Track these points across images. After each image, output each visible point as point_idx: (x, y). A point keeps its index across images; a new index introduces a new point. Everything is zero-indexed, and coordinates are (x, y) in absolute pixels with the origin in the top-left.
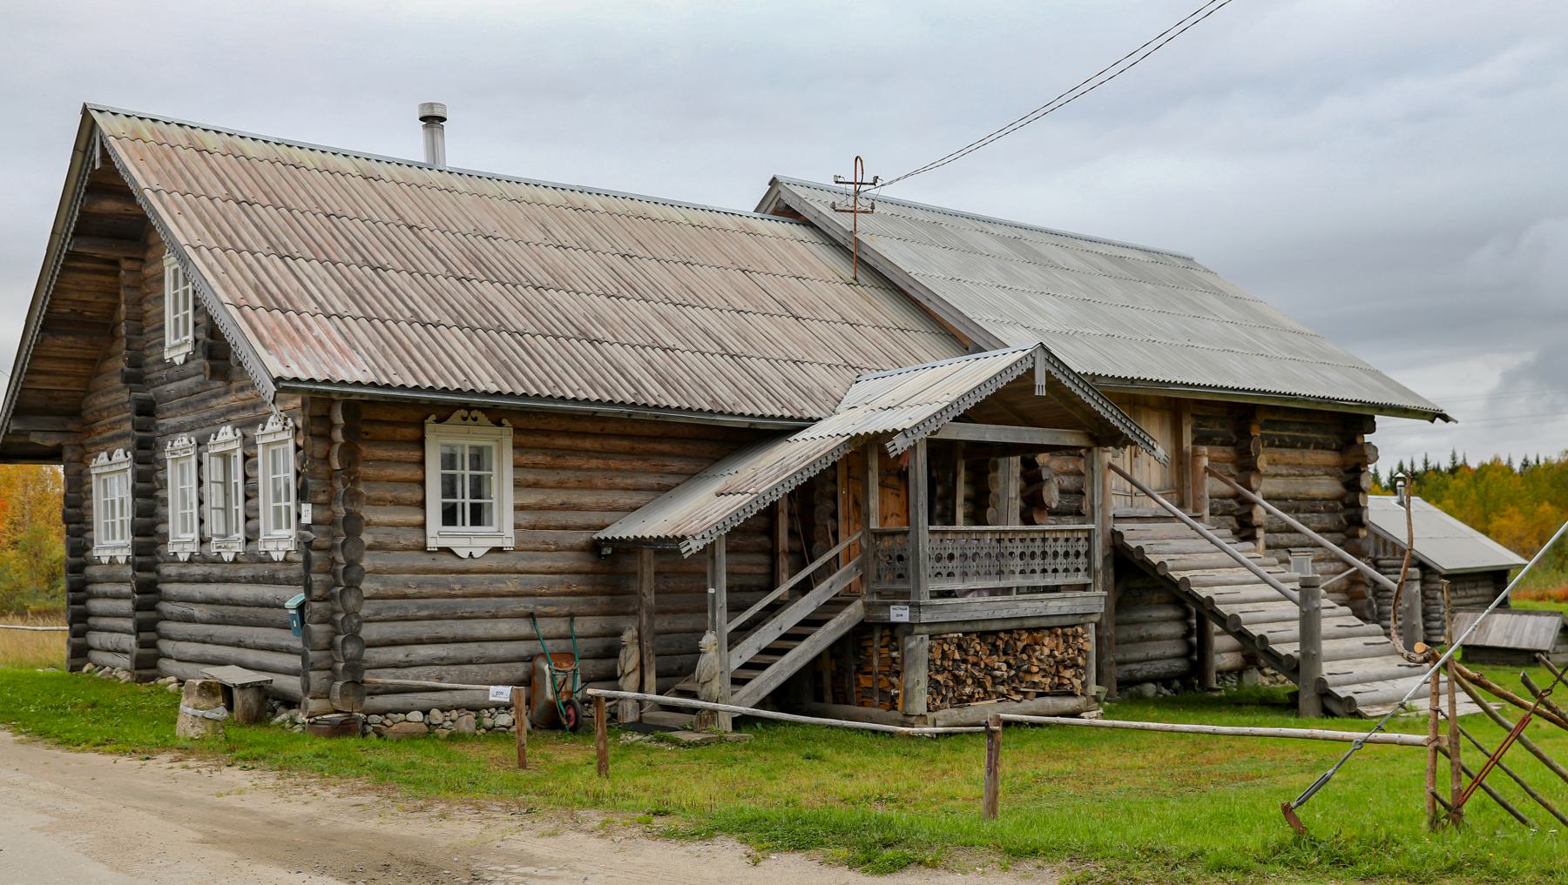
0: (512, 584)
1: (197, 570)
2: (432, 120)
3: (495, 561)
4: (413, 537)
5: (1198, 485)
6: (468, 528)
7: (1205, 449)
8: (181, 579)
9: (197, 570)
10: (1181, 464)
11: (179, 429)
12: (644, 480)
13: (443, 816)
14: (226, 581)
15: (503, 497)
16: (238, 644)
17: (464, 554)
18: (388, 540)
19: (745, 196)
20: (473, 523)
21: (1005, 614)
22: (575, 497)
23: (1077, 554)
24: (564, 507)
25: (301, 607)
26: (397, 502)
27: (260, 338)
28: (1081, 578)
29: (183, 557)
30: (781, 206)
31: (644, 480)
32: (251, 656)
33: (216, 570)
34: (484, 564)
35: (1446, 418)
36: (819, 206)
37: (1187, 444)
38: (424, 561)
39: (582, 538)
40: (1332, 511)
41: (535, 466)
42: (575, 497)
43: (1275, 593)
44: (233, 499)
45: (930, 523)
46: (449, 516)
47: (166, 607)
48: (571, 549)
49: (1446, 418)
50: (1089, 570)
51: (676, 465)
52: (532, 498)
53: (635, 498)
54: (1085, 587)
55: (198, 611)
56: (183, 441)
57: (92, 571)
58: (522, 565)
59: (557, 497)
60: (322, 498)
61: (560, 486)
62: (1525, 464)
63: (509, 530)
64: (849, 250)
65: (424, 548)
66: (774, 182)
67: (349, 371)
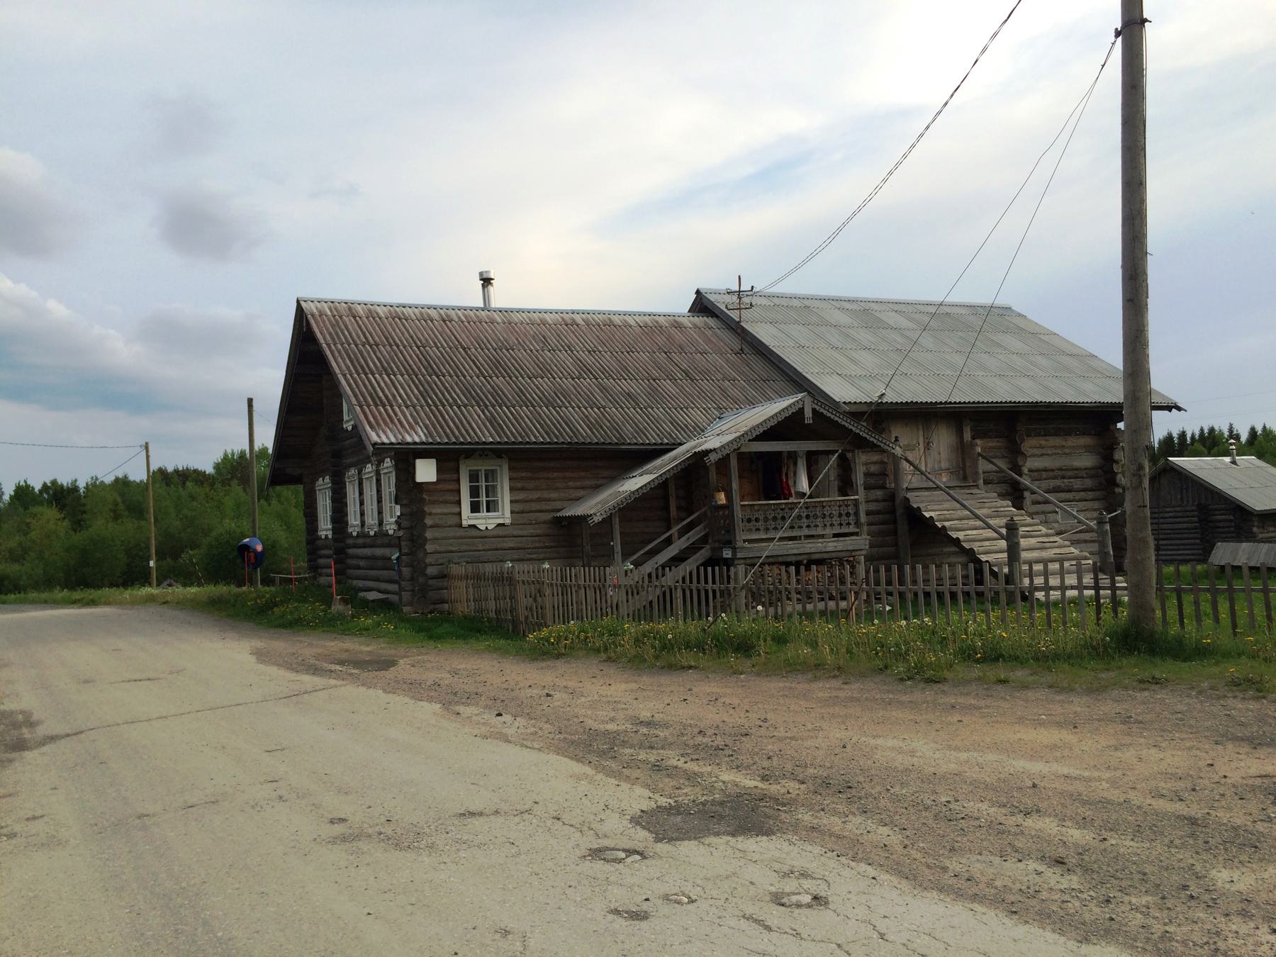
0: (510, 543)
1: (360, 541)
2: (486, 281)
3: (501, 531)
4: (453, 520)
5: (975, 464)
6: (485, 514)
7: (979, 442)
8: (356, 546)
9: (360, 541)
10: (962, 450)
11: (351, 466)
12: (587, 483)
13: (170, 585)
14: (371, 546)
15: (505, 498)
16: (377, 580)
17: (483, 528)
18: (440, 522)
19: (682, 305)
20: (488, 511)
21: (795, 551)
22: (546, 495)
23: (848, 515)
24: (539, 500)
25: (398, 559)
26: (446, 502)
27: (369, 423)
28: (852, 529)
29: (355, 534)
30: (702, 305)
31: (587, 483)
32: (383, 586)
33: (368, 540)
34: (495, 533)
35: (1179, 409)
36: (721, 302)
37: (967, 435)
38: (460, 532)
39: (549, 516)
40: (1091, 477)
41: (522, 478)
42: (546, 495)
43: (995, 535)
44: (371, 506)
45: (742, 499)
46: (475, 508)
47: (350, 561)
48: (545, 522)
49: (1179, 409)
50: (858, 524)
51: (606, 473)
52: (521, 496)
53: (582, 493)
54: (856, 534)
55: (362, 563)
56: (353, 471)
57: (319, 543)
58: (515, 533)
59: (535, 495)
60: (405, 502)
61: (536, 489)
62: (1253, 432)
63: (508, 514)
64: (737, 329)
65: (460, 525)
66: (698, 292)
67: (388, 437)
